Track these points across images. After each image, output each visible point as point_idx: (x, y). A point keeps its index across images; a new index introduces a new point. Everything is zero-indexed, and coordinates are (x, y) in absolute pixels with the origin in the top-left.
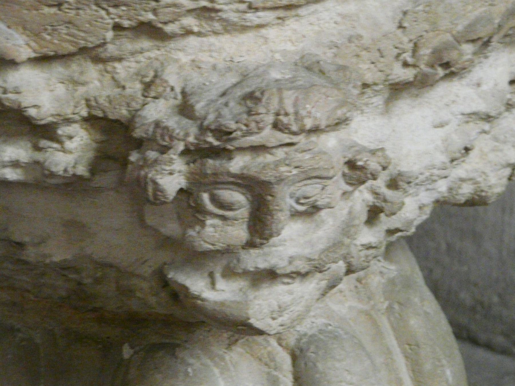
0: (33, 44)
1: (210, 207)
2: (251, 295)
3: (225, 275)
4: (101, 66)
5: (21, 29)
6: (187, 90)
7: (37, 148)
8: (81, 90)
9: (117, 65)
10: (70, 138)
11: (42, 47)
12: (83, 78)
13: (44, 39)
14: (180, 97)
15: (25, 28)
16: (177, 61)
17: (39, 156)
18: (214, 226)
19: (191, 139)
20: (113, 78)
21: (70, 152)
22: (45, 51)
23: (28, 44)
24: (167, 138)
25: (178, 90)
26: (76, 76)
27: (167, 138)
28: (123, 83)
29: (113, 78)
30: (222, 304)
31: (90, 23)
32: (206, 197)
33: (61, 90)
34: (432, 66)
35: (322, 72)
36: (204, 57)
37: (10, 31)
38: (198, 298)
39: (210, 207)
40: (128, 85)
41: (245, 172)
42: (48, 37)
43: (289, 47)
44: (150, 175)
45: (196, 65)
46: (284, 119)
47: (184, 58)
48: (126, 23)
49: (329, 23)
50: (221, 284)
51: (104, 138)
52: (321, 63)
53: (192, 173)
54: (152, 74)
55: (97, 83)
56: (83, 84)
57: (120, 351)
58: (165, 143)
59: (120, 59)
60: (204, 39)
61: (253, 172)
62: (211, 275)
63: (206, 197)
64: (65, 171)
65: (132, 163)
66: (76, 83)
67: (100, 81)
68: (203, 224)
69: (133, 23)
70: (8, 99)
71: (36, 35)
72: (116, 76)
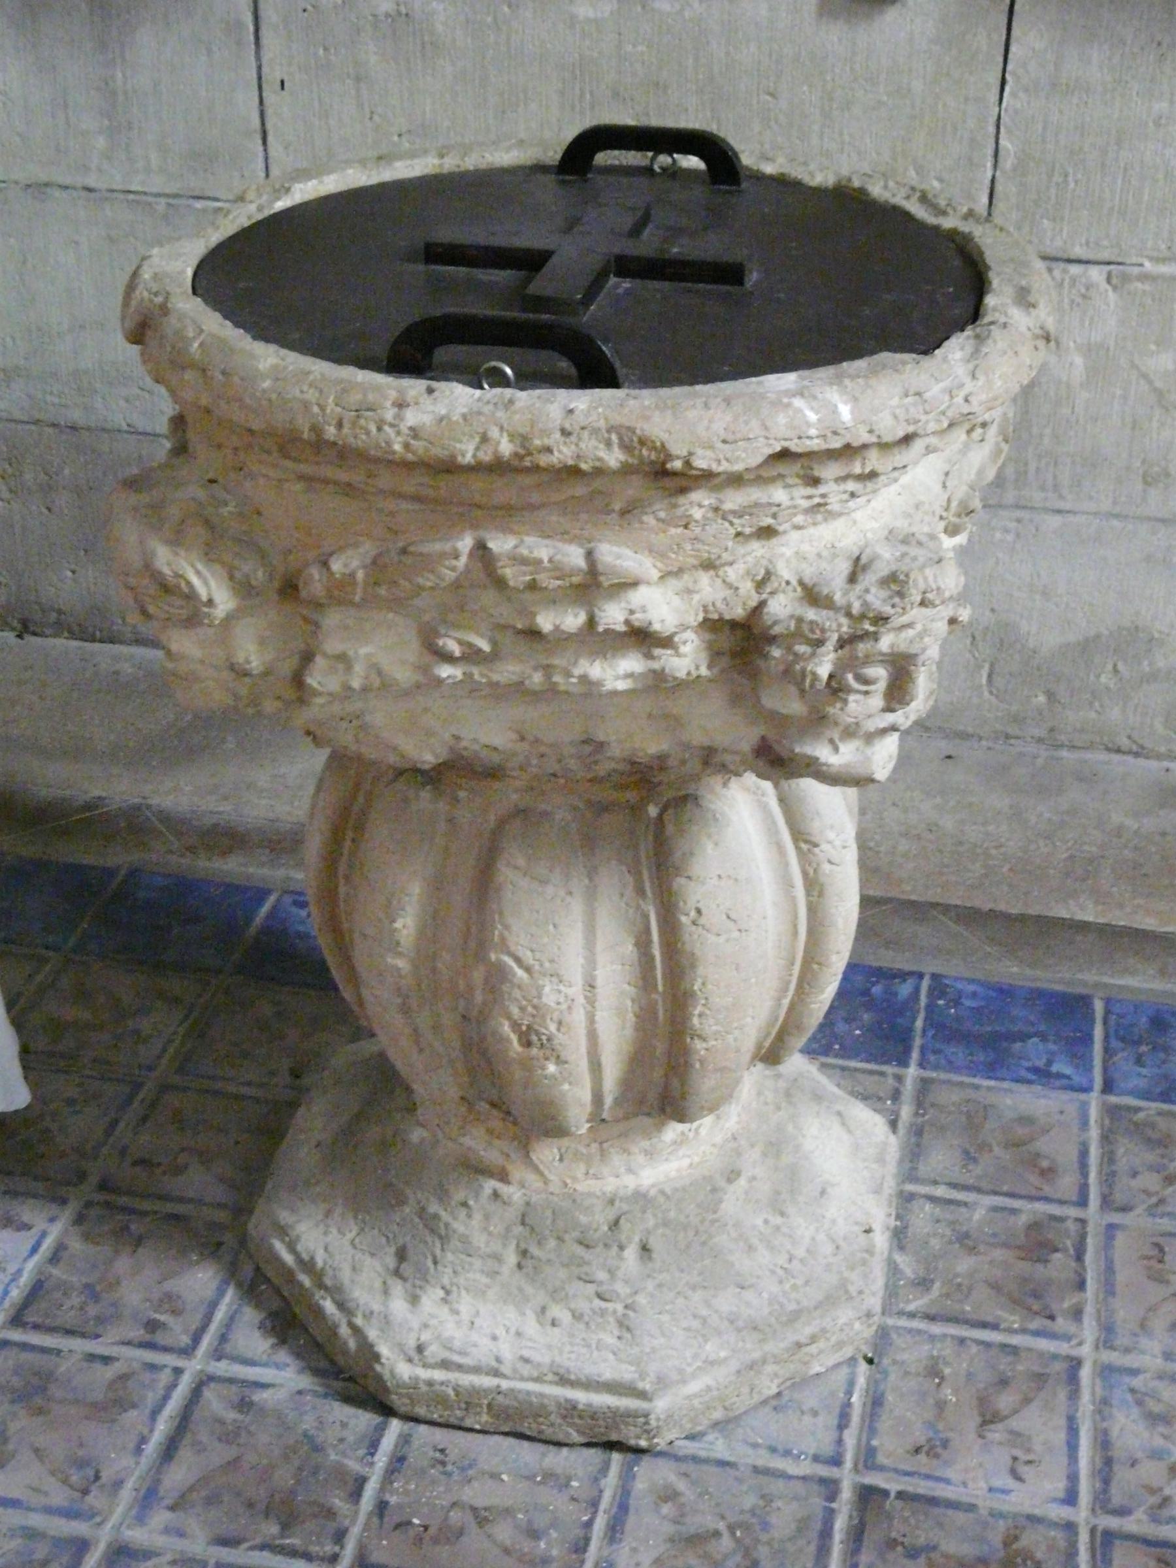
0: (659, 564)
1: (855, 685)
2: (869, 751)
3: (842, 739)
4: (712, 572)
5: (646, 553)
6: (807, 580)
7: (649, 656)
8: (696, 597)
9: (727, 568)
10: (685, 643)
11: (667, 566)
12: (697, 589)
13: (668, 558)
14: (799, 589)
15: (651, 551)
16: (782, 555)
17: (656, 665)
18: (856, 701)
19: (845, 629)
20: (724, 581)
21: (685, 656)
22: (670, 569)
23: (655, 566)
24: (818, 632)
25: (794, 582)
26: (690, 585)
27: (818, 632)
28: (736, 584)
29: (724, 581)
30: (847, 765)
31: (714, 537)
32: (850, 677)
33: (676, 601)
34: (959, 516)
35: (920, 543)
36: (806, 548)
37: (638, 556)
38: (825, 764)
39: (855, 685)
40: (740, 585)
41: (896, 649)
42: (673, 556)
43: (875, 525)
44: (809, 668)
45: (801, 557)
46: (930, 596)
47: (788, 552)
48: (748, 531)
49: (398, 433)
50: (843, 748)
51: (713, 637)
52: (917, 535)
53: (838, 659)
54: (762, 572)
55: (709, 589)
56: (697, 592)
57: (647, 811)
58: (815, 636)
59: (731, 564)
60: (805, 531)
61: (903, 647)
62: (831, 741)
63: (850, 677)
64: (689, 674)
65: (775, 658)
66: (689, 592)
67: (711, 586)
68: (845, 702)
69: (754, 530)
70: (637, 619)
71: (662, 556)
72: (728, 580)
